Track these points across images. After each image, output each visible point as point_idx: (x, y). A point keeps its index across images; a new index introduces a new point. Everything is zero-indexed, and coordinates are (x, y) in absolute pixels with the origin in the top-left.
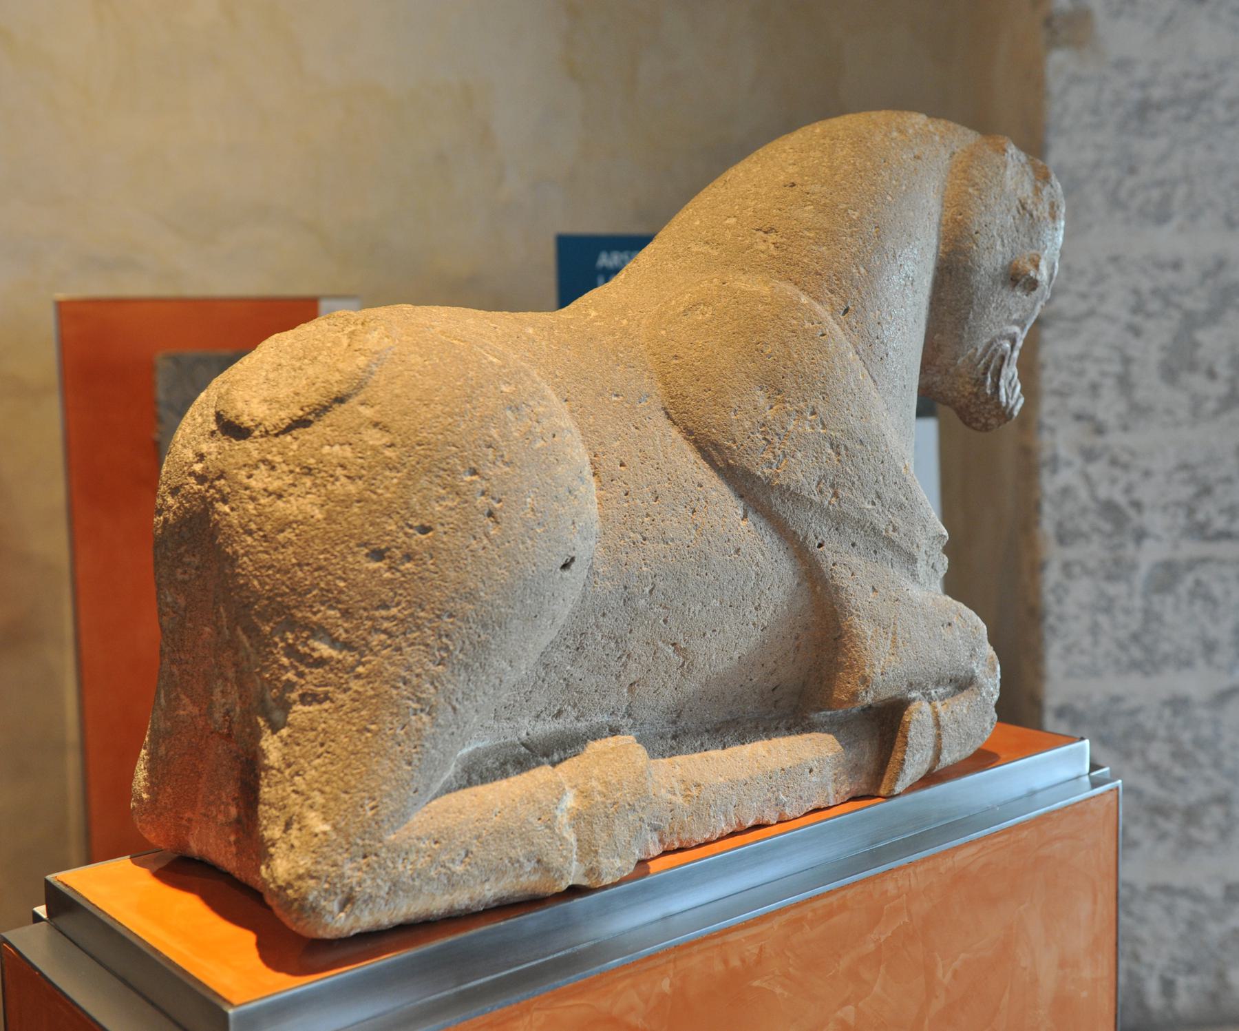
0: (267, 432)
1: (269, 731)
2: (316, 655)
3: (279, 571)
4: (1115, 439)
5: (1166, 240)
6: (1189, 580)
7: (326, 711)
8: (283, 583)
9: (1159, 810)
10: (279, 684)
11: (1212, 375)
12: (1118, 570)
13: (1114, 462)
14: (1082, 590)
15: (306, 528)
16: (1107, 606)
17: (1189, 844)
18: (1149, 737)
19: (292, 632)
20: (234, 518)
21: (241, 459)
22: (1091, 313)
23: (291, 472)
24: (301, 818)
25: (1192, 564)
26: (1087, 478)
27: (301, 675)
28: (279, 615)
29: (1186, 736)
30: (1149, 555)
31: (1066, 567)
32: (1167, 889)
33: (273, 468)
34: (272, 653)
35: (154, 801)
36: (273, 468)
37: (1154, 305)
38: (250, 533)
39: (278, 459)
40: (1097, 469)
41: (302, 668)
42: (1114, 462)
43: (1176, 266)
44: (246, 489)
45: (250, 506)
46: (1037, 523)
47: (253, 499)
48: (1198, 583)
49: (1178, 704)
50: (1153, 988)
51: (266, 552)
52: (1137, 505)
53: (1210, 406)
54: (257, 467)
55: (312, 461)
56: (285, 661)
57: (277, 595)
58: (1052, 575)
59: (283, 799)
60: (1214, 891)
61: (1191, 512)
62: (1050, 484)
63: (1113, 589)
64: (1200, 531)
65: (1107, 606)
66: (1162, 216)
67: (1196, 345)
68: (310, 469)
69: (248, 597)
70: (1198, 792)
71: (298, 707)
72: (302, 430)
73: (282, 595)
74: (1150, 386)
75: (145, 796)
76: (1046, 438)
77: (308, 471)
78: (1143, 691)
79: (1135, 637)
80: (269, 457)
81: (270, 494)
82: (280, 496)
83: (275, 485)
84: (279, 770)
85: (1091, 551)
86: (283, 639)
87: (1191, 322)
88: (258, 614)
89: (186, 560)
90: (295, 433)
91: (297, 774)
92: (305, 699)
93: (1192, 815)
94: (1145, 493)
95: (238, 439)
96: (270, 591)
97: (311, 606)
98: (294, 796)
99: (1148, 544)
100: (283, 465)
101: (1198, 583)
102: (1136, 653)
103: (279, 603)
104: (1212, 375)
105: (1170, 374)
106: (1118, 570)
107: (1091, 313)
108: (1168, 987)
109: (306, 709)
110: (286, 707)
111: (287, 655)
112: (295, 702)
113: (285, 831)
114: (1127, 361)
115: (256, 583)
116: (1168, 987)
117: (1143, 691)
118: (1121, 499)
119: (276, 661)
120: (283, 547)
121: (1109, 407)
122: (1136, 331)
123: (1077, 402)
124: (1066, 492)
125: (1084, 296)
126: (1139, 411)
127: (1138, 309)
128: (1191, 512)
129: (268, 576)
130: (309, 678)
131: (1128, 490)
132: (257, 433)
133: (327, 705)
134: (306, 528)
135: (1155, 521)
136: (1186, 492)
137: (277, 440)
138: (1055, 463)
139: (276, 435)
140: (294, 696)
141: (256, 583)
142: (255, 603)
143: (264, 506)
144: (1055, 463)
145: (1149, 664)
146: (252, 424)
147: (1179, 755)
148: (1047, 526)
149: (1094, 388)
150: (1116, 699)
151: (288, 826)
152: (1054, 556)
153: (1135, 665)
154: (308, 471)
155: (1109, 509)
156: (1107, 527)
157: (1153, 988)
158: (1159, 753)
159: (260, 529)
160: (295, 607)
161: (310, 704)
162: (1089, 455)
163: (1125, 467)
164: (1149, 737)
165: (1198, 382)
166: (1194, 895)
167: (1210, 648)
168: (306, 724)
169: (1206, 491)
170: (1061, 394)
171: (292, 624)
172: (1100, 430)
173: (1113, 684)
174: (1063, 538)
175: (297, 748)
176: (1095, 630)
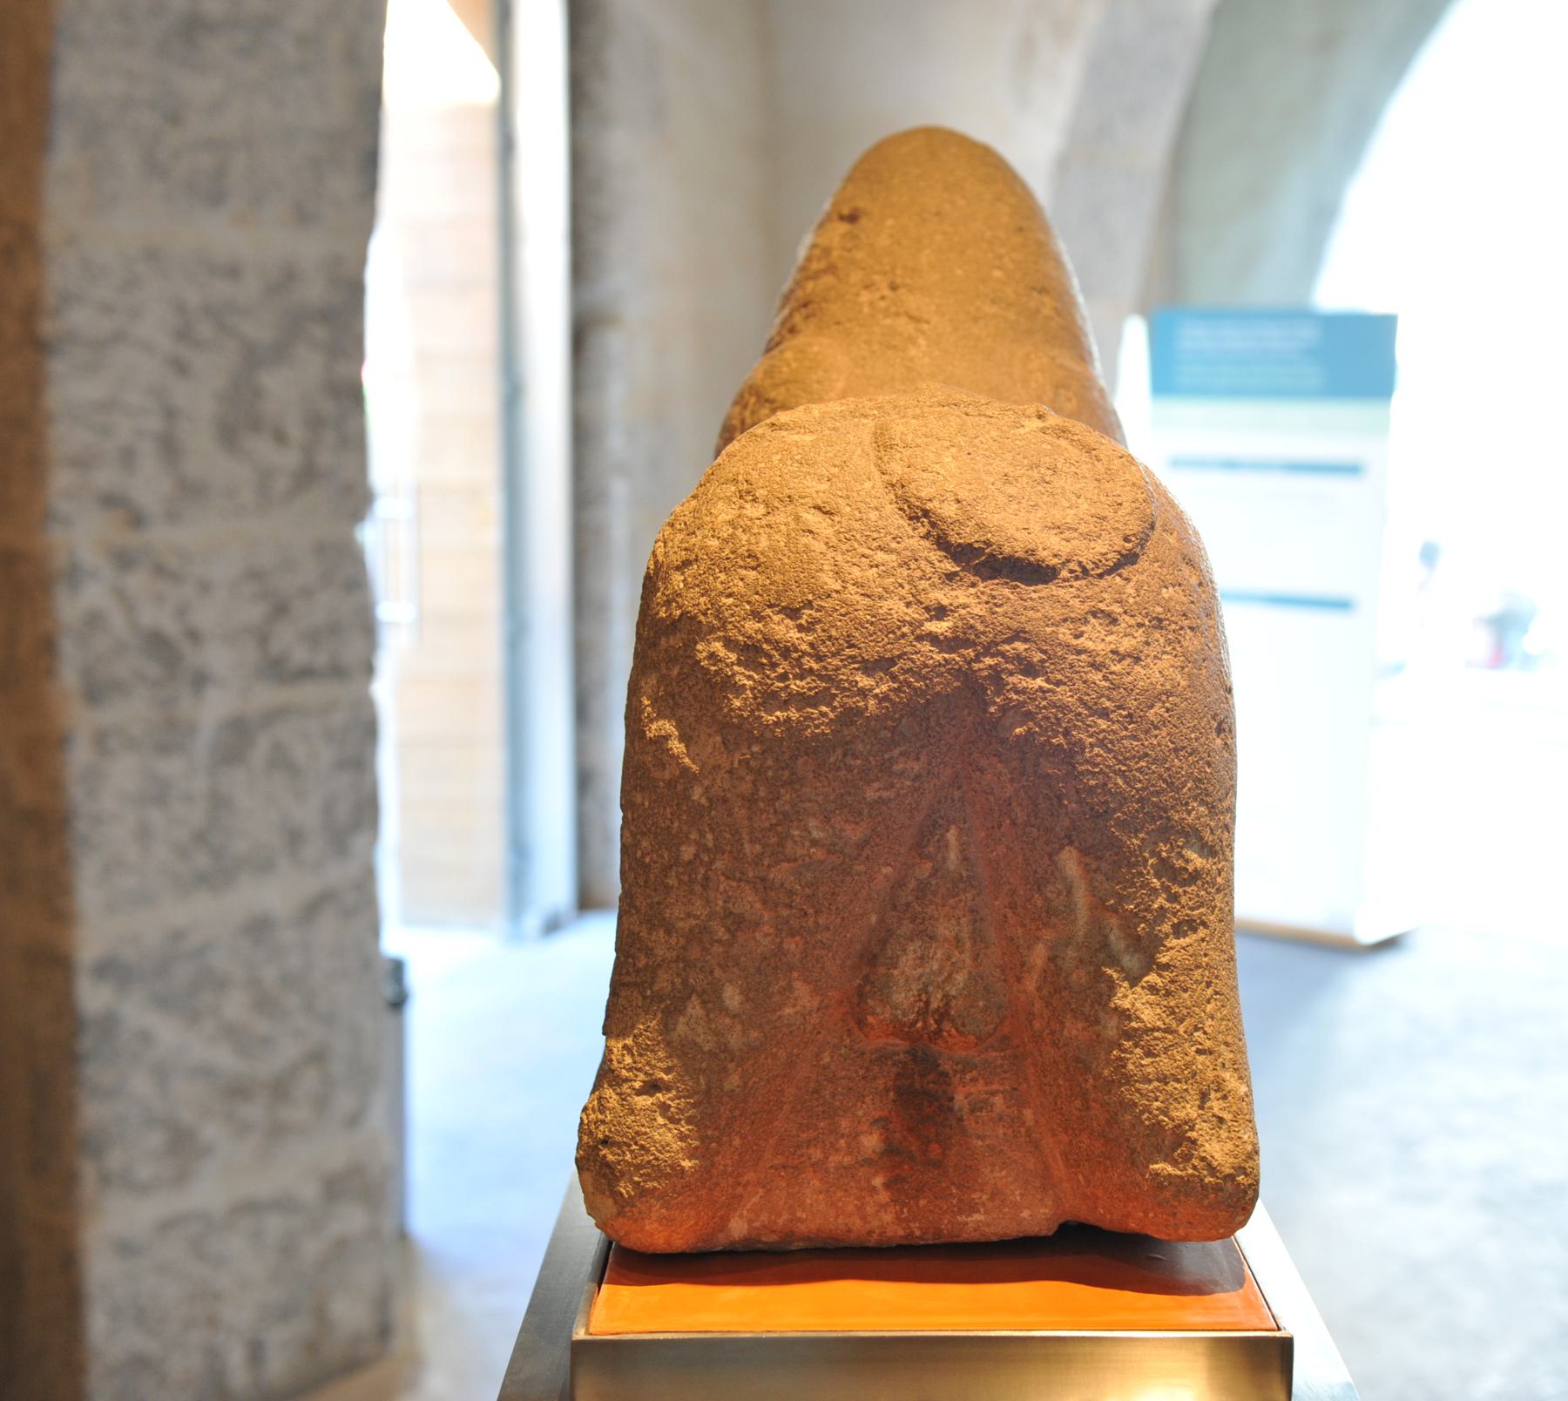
0: (1085, 571)
1: (1126, 984)
2: (1190, 868)
3: (1155, 761)
4: (160, 536)
5: (218, 233)
6: (261, 748)
7: (1203, 940)
8: (1160, 776)
9: (238, 1091)
10: (1149, 916)
11: (280, 437)
12: (171, 736)
13: (160, 570)
14: (124, 773)
15: (1177, 700)
16: (159, 793)
17: (278, 1131)
18: (221, 984)
19: (1166, 841)
20: (1064, 695)
21: (1057, 613)
22: (119, 337)
23: (1140, 625)
24: (1219, 1085)
25: (273, 716)
26: (121, 596)
27: (1174, 898)
28: (1153, 820)
29: (270, 974)
30: (212, 711)
31: (101, 741)
32: (250, 1207)
33: (1114, 621)
34: (1141, 874)
35: (706, 1172)
36: (1114, 621)
37: (205, 329)
38: (1104, 714)
39: (1117, 609)
40: (138, 582)
41: (1175, 889)
42: (160, 570)
43: (233, 272)
44: (1079, 652)
45: (1096, 677)
46: (50, 672)
47: (1096, 666)
48: (278, 747)
49: (259, 928)
50: (236, 1358)
51: (1135, 738)
52: (194, 636)
53: (281, 484)
54: (1086, 622)
55: (1159, 609)
56: (1156, 883)
57: (1152, 793)
58: (80, 755)
59: (1187, 1066)
60: (309, 1191)
61: (263, 639)
62: (70, 607)
63: (171, 767)
64: (276, 670)
65: (159, 793)
66: (215, 196)
67: (258, 393)
68: (1160, 621)
69: (1106, 802)
70: (288, 1051)
71: (1173, 942)
72: (1131, 568)
73: (1158, 793)
74: (203, 453)
75: (686, 1164)
76: (57, 536)
77: (1159, 623)
78: (210, 915)
79: (200, 838)
80: (1102, 606)
81: (1123, 658)
82: (1137, 660)
83: (1126, 645)
84: (1168, 1030)
85: (132, 711)
86: (1153, 854)
87: (254, 359)
88: (1121, 824)
89: (897, 768)
90: (1125, 572)
91: (1196, 1029)
92: (1178, 931)
93: (280, 1089)
94: (206, 616)
95: (1029, 583)
96: (1143, 789)
97: (1187, 804)
98: (1201, 1058)
99: (212, 694)
100: (1127, 618)
101: (278, 747)
102: (202, 860)
103: (1155, 805)
104: (280, 437)
105: (229, 435)
106: (171, 736)
107: (119, 337)
108: (256, 1352)
109: (1183, 942)
110: (1157, 943)
111: (1158, 876)
112: (1167, 936)
113: (1201, 1107)
114: (171, 414)
115: (1120, 781)
116: (256, 1352)
117: (210, 915)
118: (171, 627)
119: (1145, 885)
120: (1156, 728)
121: (149, 486)
122: (181, 368)
123: (105, 478)
124: (94, 620)
125: (107, 309)
126: (190, 491)
127: (183, 334)
128: (263, 639)
129: (1139, 770)
130: (1183, 900)
131: (182, 611)
132: (1064, 574)
133: (1202, 932)
134: (1177, 700)
135: (217, 657)
136: (255, 613)
137: (1103, 583)
138: (75, 575)
139: (1101, 576)
140: (1166, 928)
141: (1120, 781)
142: (1115, 811)
143: (1119, 674)
144: (75, 575)
145: (219, 877)
146: (1055, 561)
147: (264, 1003)
148: (69, 676)
149: (128, 457)
150: (178, 935)
151: (1204, 1097)
152: (83, 723)
153: (203, 880)
154: (1159, 623)
155: (157, 643)
156: (153, 669)
157: (236, 1358)
158: (236, 1006)
159: (1120, 707)
160: (1173, 807)
161: (1185, 935)
162: (124, 560)
163: (175, 577)
164: (221, 984)
165: (261, 447)
166: (284, 1204)
167: (295, 838)
168: (1190, 962)
169: (280, 610)
170: (83, 463)
171: (1168, 831)
172: (137, 520)
173: (176, 913)
174: (95, 693)
175: (1186, 995)
176: (144, 834)
